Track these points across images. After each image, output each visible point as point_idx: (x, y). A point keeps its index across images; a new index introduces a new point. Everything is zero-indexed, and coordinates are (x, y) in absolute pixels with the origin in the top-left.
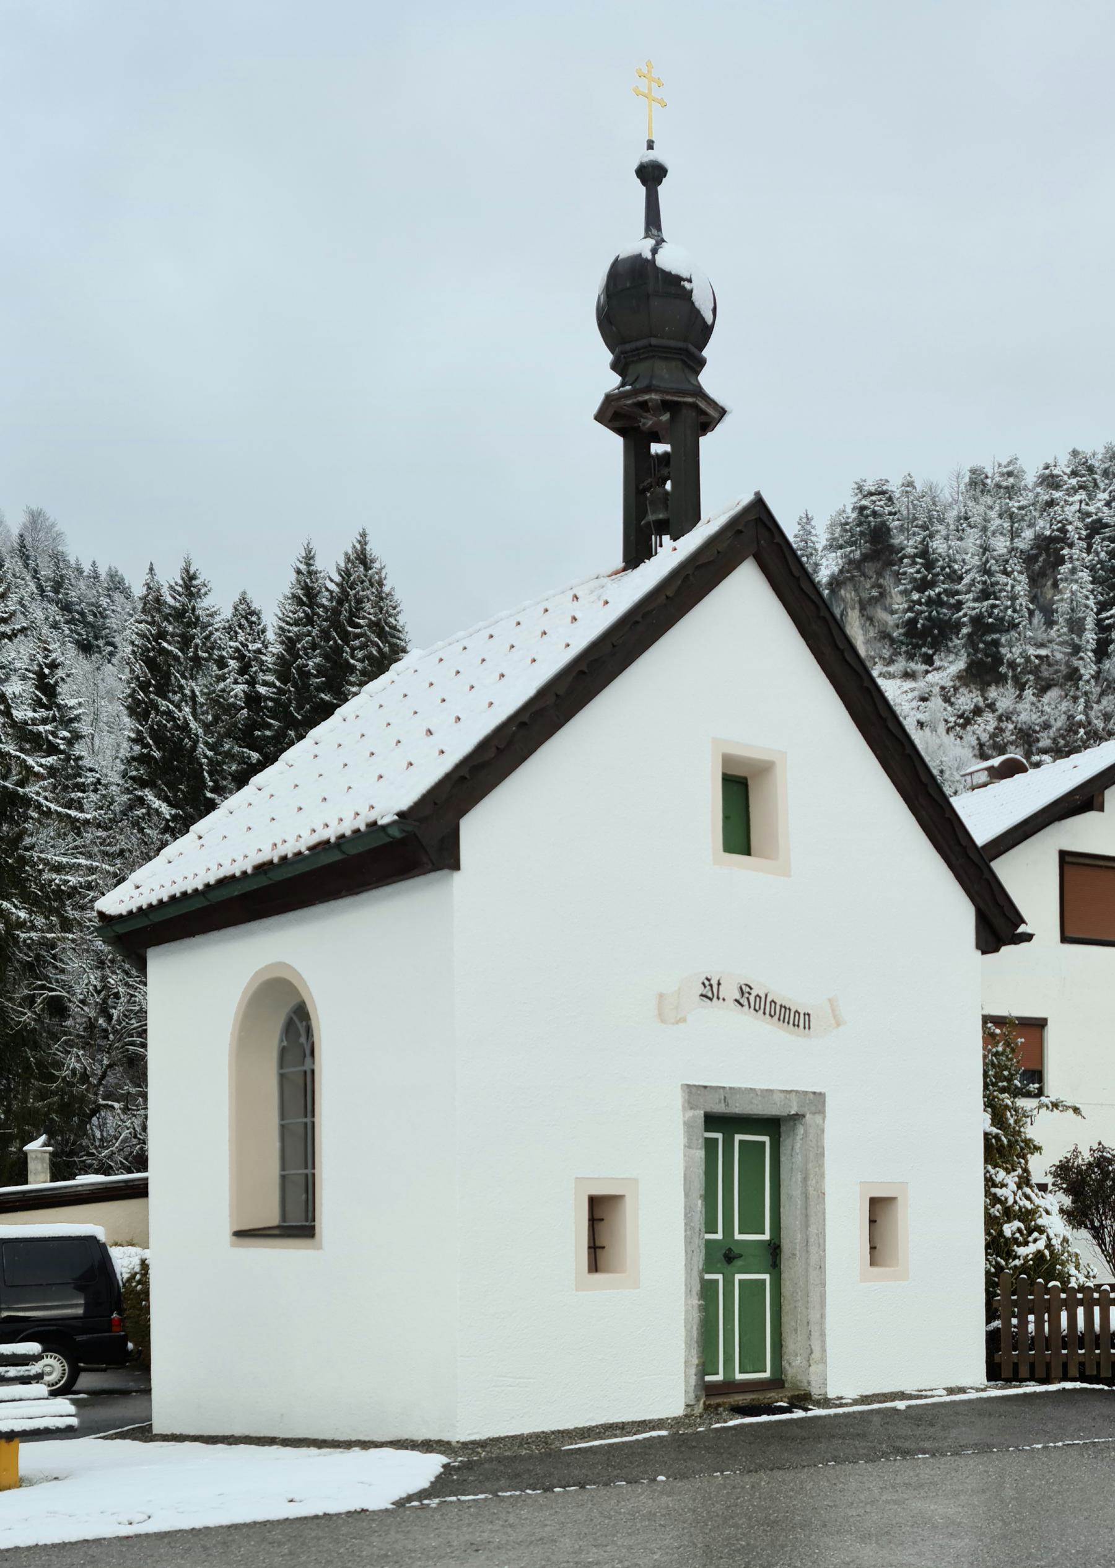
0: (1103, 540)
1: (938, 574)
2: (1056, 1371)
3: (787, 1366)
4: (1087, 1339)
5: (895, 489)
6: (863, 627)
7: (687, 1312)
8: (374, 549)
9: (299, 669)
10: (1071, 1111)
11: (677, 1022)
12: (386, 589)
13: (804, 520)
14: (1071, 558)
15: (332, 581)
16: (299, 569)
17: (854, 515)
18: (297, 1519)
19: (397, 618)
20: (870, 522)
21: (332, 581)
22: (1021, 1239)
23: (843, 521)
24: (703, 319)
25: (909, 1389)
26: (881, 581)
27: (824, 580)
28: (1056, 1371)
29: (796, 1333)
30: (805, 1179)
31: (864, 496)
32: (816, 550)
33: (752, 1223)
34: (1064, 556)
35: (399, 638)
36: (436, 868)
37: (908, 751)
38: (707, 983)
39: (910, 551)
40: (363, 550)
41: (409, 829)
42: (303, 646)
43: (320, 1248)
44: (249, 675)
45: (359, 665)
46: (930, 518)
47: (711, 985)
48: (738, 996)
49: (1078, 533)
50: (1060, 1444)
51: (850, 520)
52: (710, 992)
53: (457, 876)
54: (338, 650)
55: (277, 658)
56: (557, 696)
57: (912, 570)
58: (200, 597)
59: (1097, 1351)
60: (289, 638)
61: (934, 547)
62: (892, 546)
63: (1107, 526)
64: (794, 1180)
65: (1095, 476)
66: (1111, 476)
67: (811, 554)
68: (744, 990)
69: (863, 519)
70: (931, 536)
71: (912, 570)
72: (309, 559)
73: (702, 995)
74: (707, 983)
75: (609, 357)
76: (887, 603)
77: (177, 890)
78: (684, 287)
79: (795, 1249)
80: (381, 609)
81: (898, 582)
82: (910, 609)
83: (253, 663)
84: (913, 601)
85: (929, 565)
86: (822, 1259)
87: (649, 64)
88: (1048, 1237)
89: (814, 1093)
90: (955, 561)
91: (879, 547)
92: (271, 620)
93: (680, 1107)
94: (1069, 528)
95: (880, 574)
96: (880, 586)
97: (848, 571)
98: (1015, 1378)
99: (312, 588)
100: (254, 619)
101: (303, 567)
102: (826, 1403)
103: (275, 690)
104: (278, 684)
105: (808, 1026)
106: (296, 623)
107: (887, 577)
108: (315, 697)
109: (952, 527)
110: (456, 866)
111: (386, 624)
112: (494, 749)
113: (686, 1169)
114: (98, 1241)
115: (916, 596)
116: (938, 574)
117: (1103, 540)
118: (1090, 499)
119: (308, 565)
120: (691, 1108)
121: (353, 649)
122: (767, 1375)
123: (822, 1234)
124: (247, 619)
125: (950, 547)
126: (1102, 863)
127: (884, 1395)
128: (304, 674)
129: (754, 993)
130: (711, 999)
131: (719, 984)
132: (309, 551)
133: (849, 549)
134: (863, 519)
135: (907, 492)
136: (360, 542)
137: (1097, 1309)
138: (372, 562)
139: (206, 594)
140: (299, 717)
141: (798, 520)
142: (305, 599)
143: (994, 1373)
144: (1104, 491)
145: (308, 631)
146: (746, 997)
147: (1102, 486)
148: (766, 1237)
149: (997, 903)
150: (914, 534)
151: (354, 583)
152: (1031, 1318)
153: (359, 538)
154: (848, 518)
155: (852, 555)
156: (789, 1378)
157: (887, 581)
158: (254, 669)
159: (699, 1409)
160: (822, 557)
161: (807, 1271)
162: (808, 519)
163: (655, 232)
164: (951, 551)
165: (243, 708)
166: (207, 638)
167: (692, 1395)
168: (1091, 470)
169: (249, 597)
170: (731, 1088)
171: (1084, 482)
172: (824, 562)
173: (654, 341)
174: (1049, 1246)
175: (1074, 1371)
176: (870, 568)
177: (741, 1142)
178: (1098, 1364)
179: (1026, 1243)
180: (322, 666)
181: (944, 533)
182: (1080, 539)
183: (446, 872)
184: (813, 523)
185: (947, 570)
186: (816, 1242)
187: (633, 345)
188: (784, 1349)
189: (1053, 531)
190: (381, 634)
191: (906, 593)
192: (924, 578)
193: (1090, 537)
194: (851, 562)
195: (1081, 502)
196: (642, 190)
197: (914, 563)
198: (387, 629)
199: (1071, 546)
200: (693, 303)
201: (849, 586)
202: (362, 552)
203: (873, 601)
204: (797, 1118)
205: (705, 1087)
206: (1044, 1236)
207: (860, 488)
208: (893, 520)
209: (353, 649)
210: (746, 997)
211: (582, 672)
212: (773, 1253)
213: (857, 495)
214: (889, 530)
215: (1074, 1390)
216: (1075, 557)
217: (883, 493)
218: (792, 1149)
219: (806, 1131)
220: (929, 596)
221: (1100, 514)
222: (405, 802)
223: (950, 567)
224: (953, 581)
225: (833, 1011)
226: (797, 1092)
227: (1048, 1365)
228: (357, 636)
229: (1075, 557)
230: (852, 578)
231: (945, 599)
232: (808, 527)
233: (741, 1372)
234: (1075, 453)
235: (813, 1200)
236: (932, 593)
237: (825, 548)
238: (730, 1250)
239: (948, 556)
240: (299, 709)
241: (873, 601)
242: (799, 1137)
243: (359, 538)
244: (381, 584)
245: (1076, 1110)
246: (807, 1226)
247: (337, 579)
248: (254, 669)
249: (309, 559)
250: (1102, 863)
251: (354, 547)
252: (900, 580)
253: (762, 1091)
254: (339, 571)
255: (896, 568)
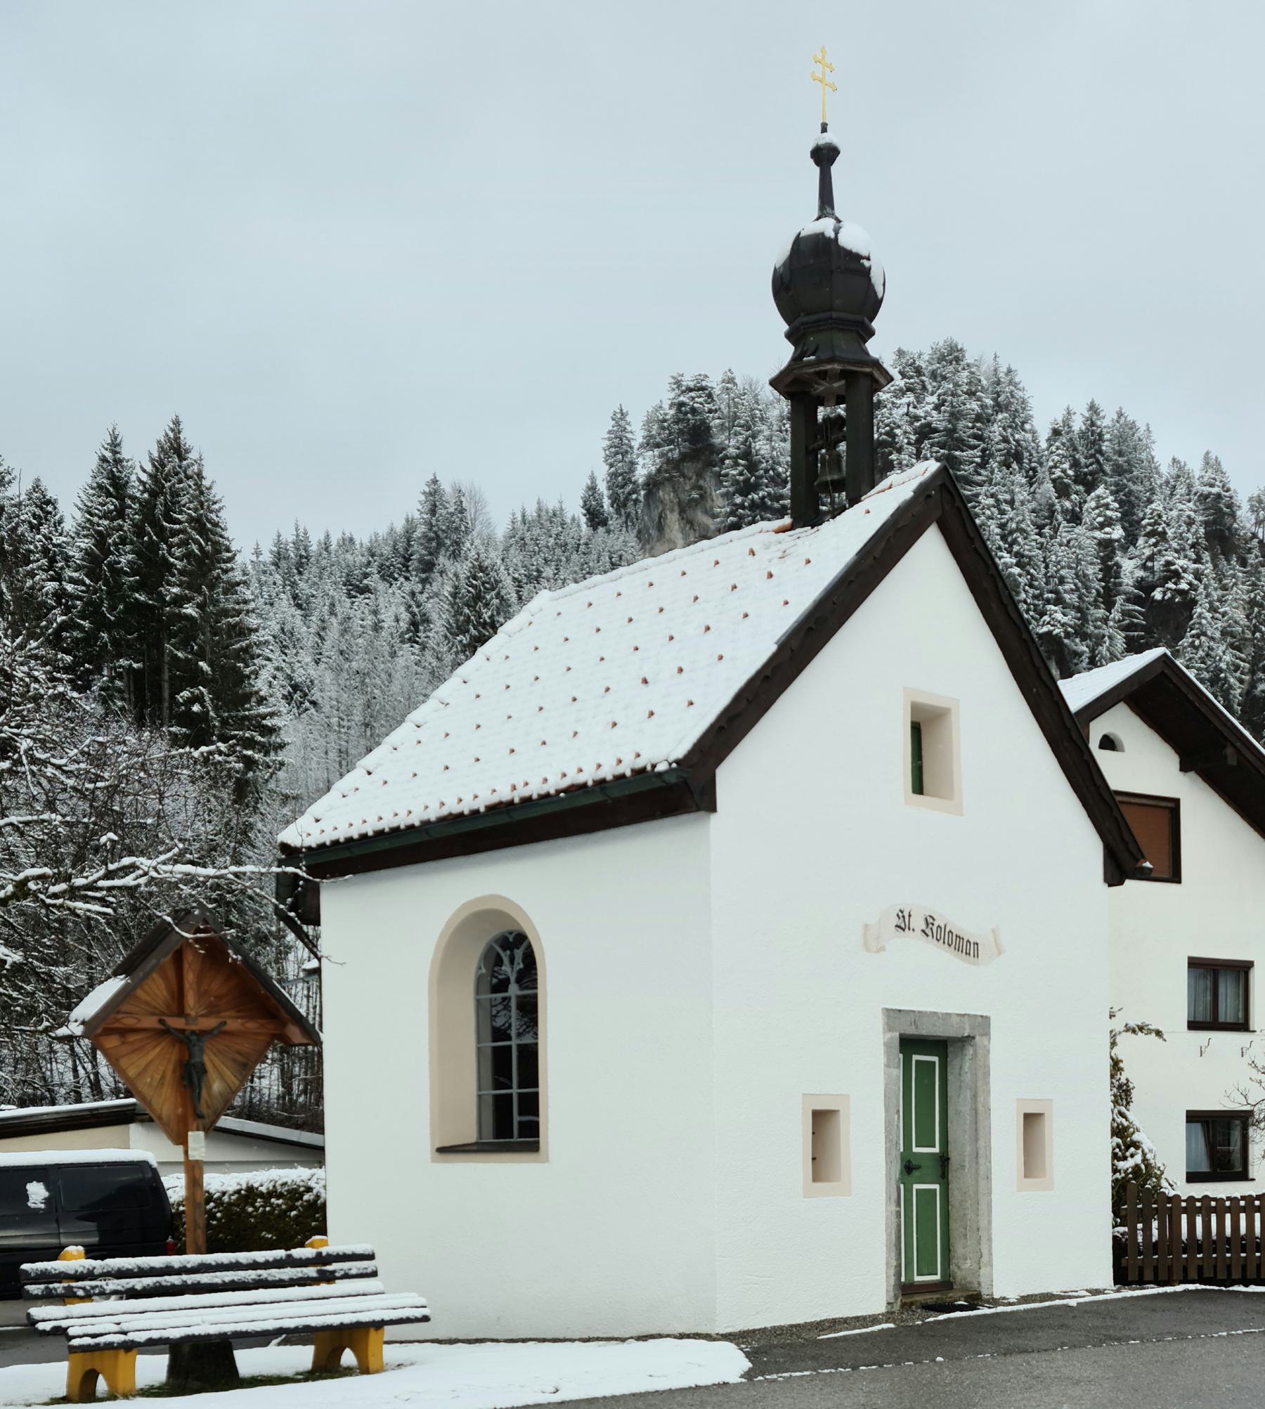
0: (932, 445)
1: (762, 477)
2: (1178, 1274)
3: (956, 1270)
4: (1205, 1246)
5: (715, 386)
6: (682, 531)
7: (887, 1217)
8: (188, 438)
9: (110, 565)
10: (1153, 1034)
11: (878, 951)
12: (206, 483)
13: (619, 416)
14: (900, 463)
15: (144, 471)
16: (104, 456)
17: (672, 412)
18: (677, 1390)
19: (219, 514)
20: (689, 420)
21: (144, 471)
22: (1120, 1154)
23: (661, 417)
24: (876, 293)
25: (1056, 1290)
26: (701, 482)
27: (641, 481)
28: (1178, 1274)
29: (966, 1238)
30: (975, 1097)
31: (683, 392)
32: (631, 447)
33: (926, 1140)
34: (892, 461)
35: (222, 536)
36: (698, 809)
37: (1056, 698)
38: (900, 915)
39: (732, 451)
40: (177, 439)
41: (685, 775)
42: (114, 541)
43: (546, 1160)
44: (55, 571)
45: (179, 565)
46: (753, 417)
47: (904, 917)
48: (924, 927)
49: (908, 438)
50: (1240, 1332)
51: (668, 417)
52: (903, 924)
53: (714, 819)
54: (153, 546)
55: (86, 554)
56: (792, 650)
57: (734, 472)
58: (4, 486)
59: (1214, 1256)
60: (99, 533)
61: (757, 448)
62: (712, 445)
63: (936, 430)
64: (962, 1096)
65: (924, 378)
66: (939, 379)
67: (627, 452)
68: (929, 921)
69: (681, 416)
70: (754, 436)
71: (734, 472)
72: (115, 446)
73: (897, 926)
74: (901, 914)
75: (785, 327)
76: (708, 505)
77: (386, 825)
78: (863, 264)
79: (964, 1161)
80: (202, 504)
81: (720, 484)
82: (732, 513)
83: (58, 558)
84: (735, 505)
85: (752, 467)
86: (989, 1170)
87: (823, 51)
88: (1143, 1151)
89: (982, 1016)
90: (779, 464)
91: (699, 446)
92: (70, 514)
93: (881, 1030)
94: (898, 431)
95: (699, 475)
96: (700, 488)
97: (666, 471)
98: (1141, 1283)
99: (119, 478)
100: (50, 508)
101: (108, 455)
102: (995, 1302)
103: (83, 588)
104: (88, 581)
105: (977, 955)
106: (105, 516)
107: (708, 479)
108: (129, 597)
109: (775, 427)
110: (711, 807)
111: (207, 520)
112: (745, 702)
113: (886, 1086)
114: (150, 1166)
115: (738, 500)
116: (762, 477)
117: (932, 445)
118: (918, 402)
119: (115, 453)
120: (890, 1030)
121: (170, 546)
122: (937, 1277)
123: (988, 1147)
124: (42, 509)
125: (773, 449)
126: (1133, 800)
127: (864, 1318)
128: (116, 571)
129: (936, 925)
130: (904, 930)
131: (910, 916)
132: (114, 437)
133: (667, 448)
134: (681, 416)
135: (727, 389)
136: (172, 430)
137: (1228, 1216)
138: (187, 451)
139: (10, 482)
140: (112, 618)
141: (612, 415)
142: (111, 489)
143: (1122, 1277)
144: (932, 394)
145: (119, 524)
146: (934, 930)
147: (930, 388)
148: (936, 1150)
149: (1123, 840)
150: (736, 434)
151: (168, 475)
152: (1140, 1226)
153: (172, 426)
154: (666, 414)
155: (670, 454)
156: (958, 1279)
157: (708, 482)
158: (59, 565)
159: (897, 1307)
160: (638, 456)
161: (977, 1181)
162: (622, 414)
163: (829, 210)
164: (775, 453)
165: (54, 608)
166: (14, 529)
167: (892, 1294)
168: (919, 371)
169: (44, 484)
170: (919, 1012)
171: (912, 384)
172: (640, 461)
173: (834, 315)
174: (1144, 1160)
175: (1193, 1274)
176: (690, 468)
177: (917, 1062)
178: (1215, 1267)
179: (1125, 1158)
180: (135, 563)
181: (767, 433)
182: (909, 443)
183: (702, 813)
184: (628, 419)
185: (771, 472)
186: (980, 1155)
187: (816, 317)
188: (952, 1254)
189: (881, 434)
190: (202, 530)
191: (727, 496)
192: (747, 481)
193: (919, 442)
194: (669, 461)
195: (909, 405)
196: (817, 170)
197: (736, 464)
198: (209, 525)
199: (900, 451)
200: (870, 279)
201: (668, 488)
202: (175, 440)
203: (693, 503)
204: (970, 1038)
205: (900, 1011)
206: (1140, 1151)
207: (678, 383)
208: (713, 418)
209: (170, 546)
210: (934, 930)
211: (810, 629)
212: (943, 1163)
213: (674, 390)
214: (709, 428)
215: (1197, 1291)
216: (905, 462)
217: (703, 389)
218: (961, 1068)
219: (975, 1052)
220: (753, 500)
221: (929, 418)
222: (681, 751)
223: (774, 470)
224: (777, 484)
225: (996, 940)
226: (969, 1015)
227: (1170, 1268)
228: (174, 533)
229: (905, 462)
230: (670, 479)
231: (769, 503)
232: (623, 423)
233: (918, 1275)
234: (901, 353)
235: (979, 1117)
236: (756, 497)
237: (641, 446)
238: (909, 1161)
239: (772, 458)
240: (112, 609)
241: (693, 503)
242: (968, 1057)
243: (172, 426)
244: (200, 475)
245: (1159, 1033)
246: (977, 1140)
247: (149, 468)
248: (59, 565)
249: (115, 446)
250: (1133, 800)
251: (167, 435)
252: (721, 482)
253: (943, 1014)
254: (152, 460)
255: (717, 469)
